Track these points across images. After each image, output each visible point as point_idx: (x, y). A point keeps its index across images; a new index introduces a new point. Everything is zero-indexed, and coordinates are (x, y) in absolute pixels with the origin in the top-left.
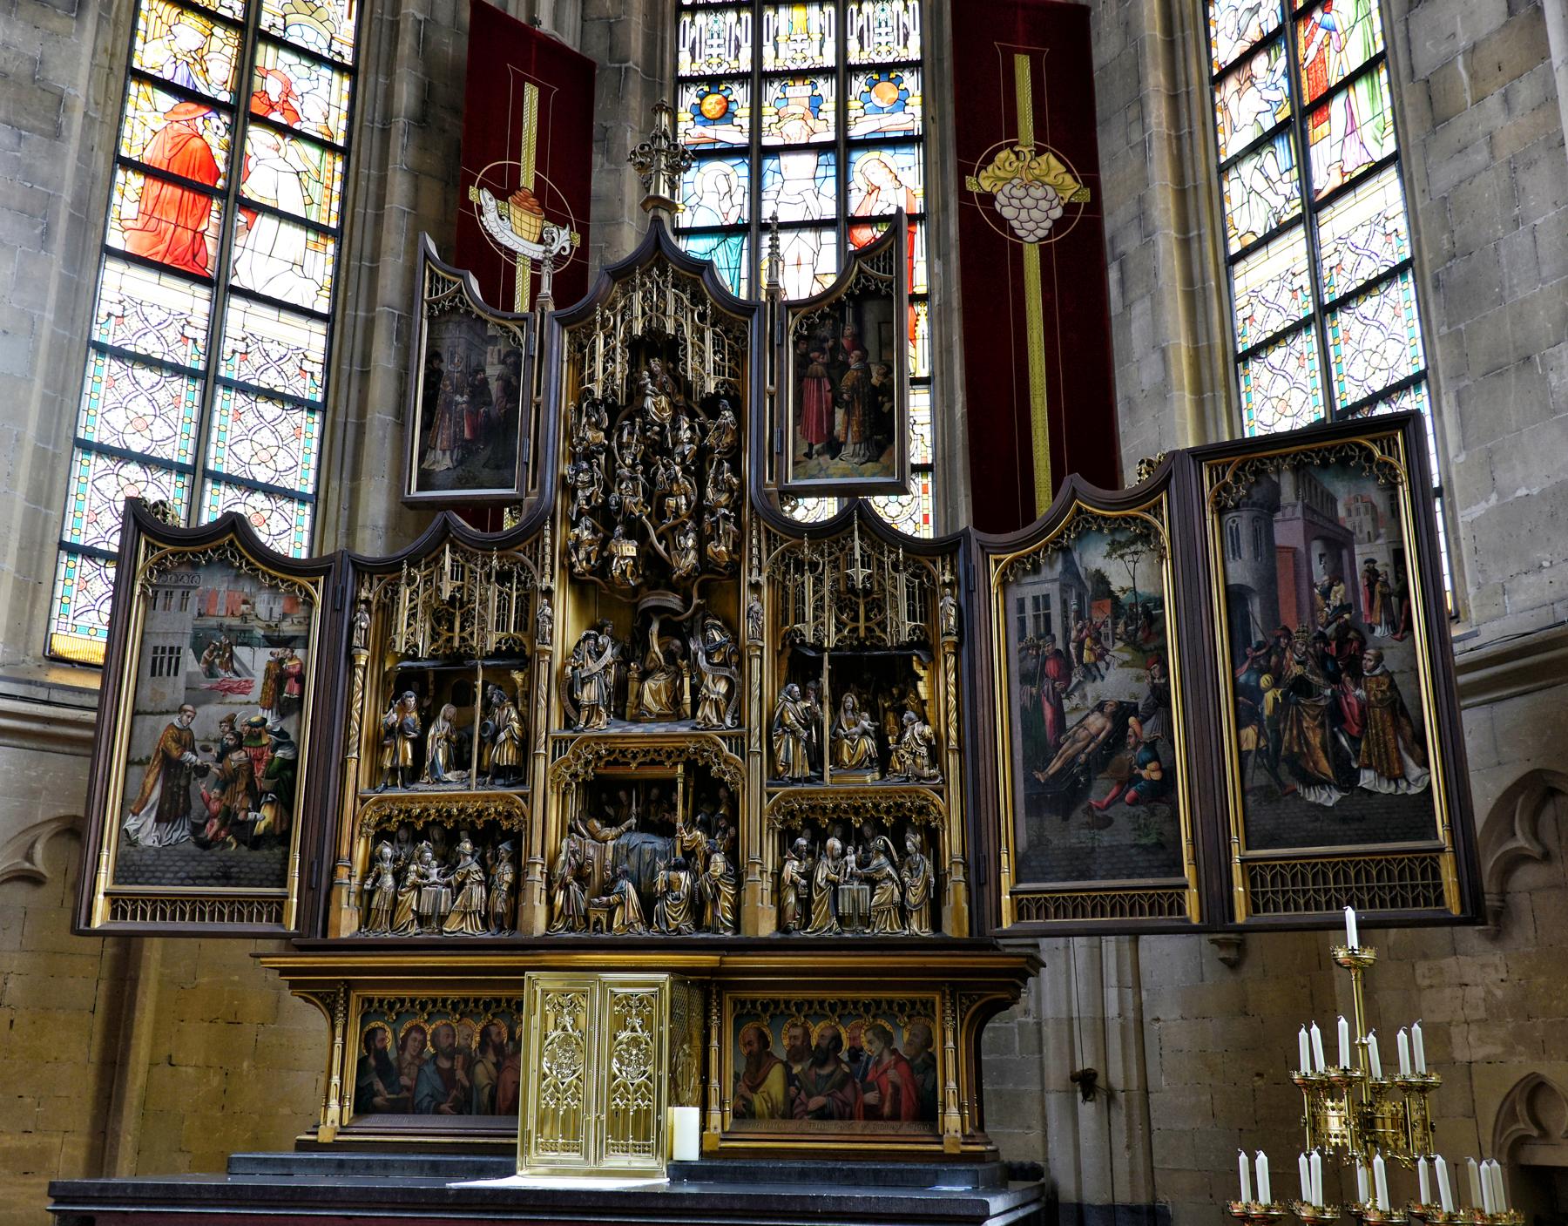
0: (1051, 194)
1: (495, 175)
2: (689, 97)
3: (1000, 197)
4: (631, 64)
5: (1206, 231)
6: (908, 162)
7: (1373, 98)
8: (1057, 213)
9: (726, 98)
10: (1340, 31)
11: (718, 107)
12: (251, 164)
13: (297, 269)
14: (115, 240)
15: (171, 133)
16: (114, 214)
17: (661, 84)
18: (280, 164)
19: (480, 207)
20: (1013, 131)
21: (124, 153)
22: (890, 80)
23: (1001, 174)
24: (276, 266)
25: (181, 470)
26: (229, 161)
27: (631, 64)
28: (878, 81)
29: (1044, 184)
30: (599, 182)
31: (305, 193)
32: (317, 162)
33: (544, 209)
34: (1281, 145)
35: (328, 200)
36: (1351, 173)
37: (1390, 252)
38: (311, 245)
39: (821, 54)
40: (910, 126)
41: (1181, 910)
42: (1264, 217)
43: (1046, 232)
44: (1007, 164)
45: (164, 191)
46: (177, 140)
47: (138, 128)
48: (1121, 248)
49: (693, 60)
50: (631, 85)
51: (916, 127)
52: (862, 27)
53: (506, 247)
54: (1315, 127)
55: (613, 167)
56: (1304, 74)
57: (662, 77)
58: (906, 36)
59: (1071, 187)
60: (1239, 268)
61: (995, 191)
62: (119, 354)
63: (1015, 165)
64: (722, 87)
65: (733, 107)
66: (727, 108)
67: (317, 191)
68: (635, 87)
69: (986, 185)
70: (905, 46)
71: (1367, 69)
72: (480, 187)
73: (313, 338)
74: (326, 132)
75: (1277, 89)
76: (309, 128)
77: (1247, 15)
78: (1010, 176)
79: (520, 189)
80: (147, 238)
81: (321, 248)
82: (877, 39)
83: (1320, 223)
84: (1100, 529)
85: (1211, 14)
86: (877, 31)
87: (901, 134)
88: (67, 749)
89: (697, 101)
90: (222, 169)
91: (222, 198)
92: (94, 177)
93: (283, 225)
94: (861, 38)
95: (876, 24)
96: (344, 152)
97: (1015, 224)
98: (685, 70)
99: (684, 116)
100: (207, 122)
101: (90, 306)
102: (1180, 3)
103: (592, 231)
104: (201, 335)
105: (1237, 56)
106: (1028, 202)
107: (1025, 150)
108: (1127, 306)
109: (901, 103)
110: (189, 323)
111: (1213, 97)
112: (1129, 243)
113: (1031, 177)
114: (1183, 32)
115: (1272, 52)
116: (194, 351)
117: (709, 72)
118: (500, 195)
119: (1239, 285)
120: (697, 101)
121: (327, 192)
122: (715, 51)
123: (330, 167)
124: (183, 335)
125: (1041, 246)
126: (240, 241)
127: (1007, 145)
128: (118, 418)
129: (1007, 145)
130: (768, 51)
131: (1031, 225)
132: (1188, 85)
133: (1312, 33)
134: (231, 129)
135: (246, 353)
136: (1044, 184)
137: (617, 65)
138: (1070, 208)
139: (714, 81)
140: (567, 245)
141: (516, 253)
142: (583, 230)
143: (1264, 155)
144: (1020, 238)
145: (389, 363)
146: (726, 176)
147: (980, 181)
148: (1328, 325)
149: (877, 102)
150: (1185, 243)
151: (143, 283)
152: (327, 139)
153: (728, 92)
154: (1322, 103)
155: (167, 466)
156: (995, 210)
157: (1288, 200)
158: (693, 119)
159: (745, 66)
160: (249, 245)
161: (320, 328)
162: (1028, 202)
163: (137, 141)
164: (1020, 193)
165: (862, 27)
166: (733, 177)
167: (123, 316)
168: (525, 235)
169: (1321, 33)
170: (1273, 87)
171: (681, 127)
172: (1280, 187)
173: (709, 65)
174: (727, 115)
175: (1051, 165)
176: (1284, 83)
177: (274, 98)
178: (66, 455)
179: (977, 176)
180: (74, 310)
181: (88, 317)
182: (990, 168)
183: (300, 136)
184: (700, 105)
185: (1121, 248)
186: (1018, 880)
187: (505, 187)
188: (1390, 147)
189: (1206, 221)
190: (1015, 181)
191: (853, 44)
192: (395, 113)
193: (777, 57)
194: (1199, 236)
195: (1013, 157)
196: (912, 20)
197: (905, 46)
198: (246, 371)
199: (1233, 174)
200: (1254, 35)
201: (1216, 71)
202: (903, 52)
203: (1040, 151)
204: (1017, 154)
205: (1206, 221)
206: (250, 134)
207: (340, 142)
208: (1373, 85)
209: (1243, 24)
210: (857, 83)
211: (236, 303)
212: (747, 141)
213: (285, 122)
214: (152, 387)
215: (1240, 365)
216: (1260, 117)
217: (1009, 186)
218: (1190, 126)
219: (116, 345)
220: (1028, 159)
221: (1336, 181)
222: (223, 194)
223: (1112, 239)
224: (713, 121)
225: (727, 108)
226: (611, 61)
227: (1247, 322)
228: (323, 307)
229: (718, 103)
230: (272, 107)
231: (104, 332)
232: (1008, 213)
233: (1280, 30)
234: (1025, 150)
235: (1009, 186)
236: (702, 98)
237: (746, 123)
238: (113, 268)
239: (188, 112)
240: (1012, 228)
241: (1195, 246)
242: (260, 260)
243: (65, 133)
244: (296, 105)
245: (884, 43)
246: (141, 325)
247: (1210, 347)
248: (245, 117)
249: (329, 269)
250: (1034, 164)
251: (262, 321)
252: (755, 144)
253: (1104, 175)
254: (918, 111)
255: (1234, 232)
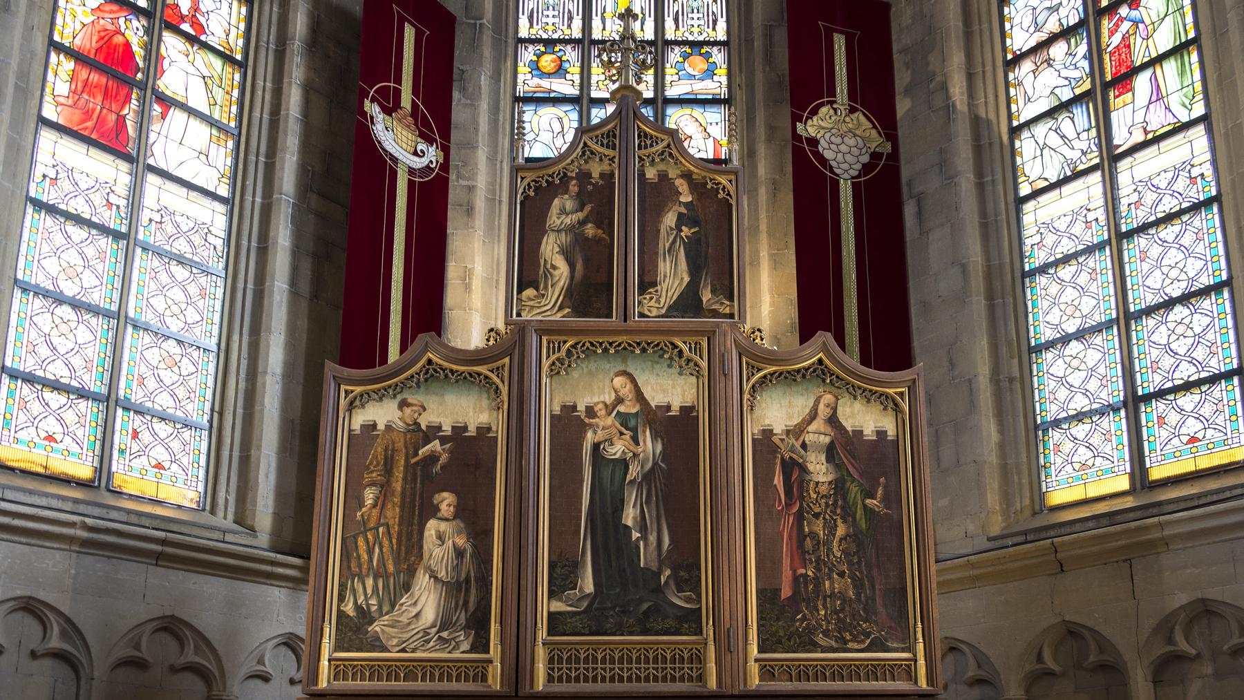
0: (861, 144)
1: (383, 92)
2: (528, 54)
3: (822, 142)
4: (485, 21)
5: (999, 177)
6: (715, 118)
7: (1182, 73)
8: (865, 159)
9: (560, 58)
10: (1148, 22)
11: (553, 65)
12: (166, 63)
13: (203, 157)
14: (49, 112)
15: (98, 28)
16: (48, 90)
17: (506, 42)
18: (191, 69)
19: (372, 118)
20: (832, 93)
21: (57, 38)
22: (701, 55)
23: (823, 124)
24: (185, 153)
25: (107, 314)
26: (147, 58)
27: (485, 21)
28: (691, 55)
29: (855, 136)
30: (459, 114)
31: (210, 96)
32: (219, 71)
33: (418, 128)
34: (1079, 113)
35: (228, 104)
36: (1155, 131)
37: (1194, 190)
38: (214, 139)
39: (642, 30)
40: (718, 91)
41: (484, 678)
42: (1058, 167)
43: (857, 173)
44: (827, 117)
45: (91, 77)
46: (103, 34)
47: (69, 19)
48: (918, 188)
49: (531, 26)
50: (485, 37)
51: (723, 92)
52: (678, 12)
53: (390, 154)
54: (1116, 97)
55: (469, 102)
56: (1107, 58)
57: (506, 37)
58: (715, 22)
59: (876, 141)
60: (1028, 207)
61: (818, 136)
62: (52, 210)
63: (833, 118)
64: (557, 49)
65: (566, 65)
66: (560, 67)
67: (219, 94)
68: (487, 38)
69: (812, 131)
70: (714, 29)
71: (1178, 50)
72: (372, 101)
73: (216, 218)
74: (227, 47)
75: (1076, 68)
76: (213, 41)
77: (1045, 13)
78: (831, 126)
79: (401, 108)
80: (77, 115)
81: (222, 143)
82: (690, 22)
83: (1119, 170)
84: (606, 350)
85: (1006, 13)
86: (690, 15)
87: (710, 97)
88: (24, 540)
89: (535, 58)
90: (141, 64)
91: (141, 89)
92: (33, 54)
93: (192, 120)
94: (676, 20)
95: (690, 10)
96: (242, 65)
97: (833, 164)
98: (523, 33)
99: (523, 70)
100: (128, 23)
101: (28, 166)
102: (978, 2)
103: (452, 152)
104: (123, 203)
105: (1034, 44)
106: (843, 148)
107: (842, 108)
108: (924, 232)
109: (710, 73)
110: (113, 191)
111: (1006, 76)
112: (931, 184)
113: (845, 129)
114: (980, 25)
115: (1073, 41)
116: (118, 216)
117: (545, 36)
118: (387, 111)
119: (1027, 219)
120: (535, 58)
121: (228, 97)
122: (550, 21)
123: (230, 77)
124: (108, 200)
125: (853, 184)
126: (155, 127)
127: (828, 102)
128: (52, 265)
129: (828, 102)
130: (596, 23)
131: (845, 166)
132: (984, 66)
133: (1117, 26)
134: (148, 31)
135: (161, 223)
136: (855, 136)
137: (472, 21)
138: (875, 156)
139: (550, 43)
140: (434, 159)
141: (397, 159)
142: (446, 150)
143: (1060, 119)
144: (838, 175)
145: (286, 241)
146: (560, 119)
147: (807, 128)
148: (1125, 246)
149: (690, 70)
150: (980, 186)
151: (72, 153)
152: (228, 53)
153: (562, 53)
154: (1124, 80)
155: (680, 102)
156: (818, 151)
157: (1084, 153)
158: (530, 72)
159: (577, 33)
160: (164, 132)
161: (221, 208)
162: (843, 148)
163: (68, 31)
164: (838, 140)
165: (678, 12)
166: (566, 121)
167: (56, 179)
168: (404, 146)
169: (1126, 26)
170: (1072, 67)
171: (521, 78)
172: (1076, 143)
173: (546, 31)
174: (560, 71)
175: (860, 119)
176: (1086, 64)
177: (185, 11)
178: (8, 292)
179: (805, 124)
180: (16, 166)
181: (27, 175)
182: (815, 118)
183: (205, 46)
184: (537, 62)
185: (918, 188)
186: (338, 648)
187: (390, 106)
188: (1199, 110)
189: (998, 169)
190: (834, 131)
191: (669, 23)
192: (289, 36)
193: (604, 29)
194: (993, 181)
195: (832, 112)
196: (719, 8)
197: (714, 29)
198: (161, 238)
199: (1025, 134)
200: (1052, 26)
201: (1010, 57)
202: (712, 34)
203: (852, 110)
204: (835, 110)
205: (998, 169)
206: (163, 38)
207: (239, 57)
208: (1183, 64)
209: (1040, 20)
210: (673, 55)
211: (151, 178)
212: (577, 92)
213: (194, 33)
214: (82, 242)
215: (1027, 280)
216: (1056, 91)
217: (829, 134)
218: (986, 98)
219: (51, 202)
220: (843, 115)
221: (1139, 137)
222: (143, 86)
223: (910, 183)
224: (549, 75)
225: (560, 67)
226: (467, 17)
227: (1036, 247)
228: (224, 191)
229: (553, 61)
230: (183, 18)
231: (40, 190)
232: (828, 155)
233: (1082, 24)
234: (842, 108)
235: (829, 134)
236: (539, 57)
237: (577, 78)
238: (47, 138)
239: (112, 12)
240: (831, 167)
241: (989, 188)
242: (172, 147)
243: (13, 8)
244: (202, 20)
245: (696, 26)
246: (72, 189)
247: (1001, 265)
248: (161, 24)
249: (229, 161)
250: (848, 119)
251: (174, 197)
252: (585, 95)
253: (901, 132)
254: (724, 80)
255: (1024, 179)
